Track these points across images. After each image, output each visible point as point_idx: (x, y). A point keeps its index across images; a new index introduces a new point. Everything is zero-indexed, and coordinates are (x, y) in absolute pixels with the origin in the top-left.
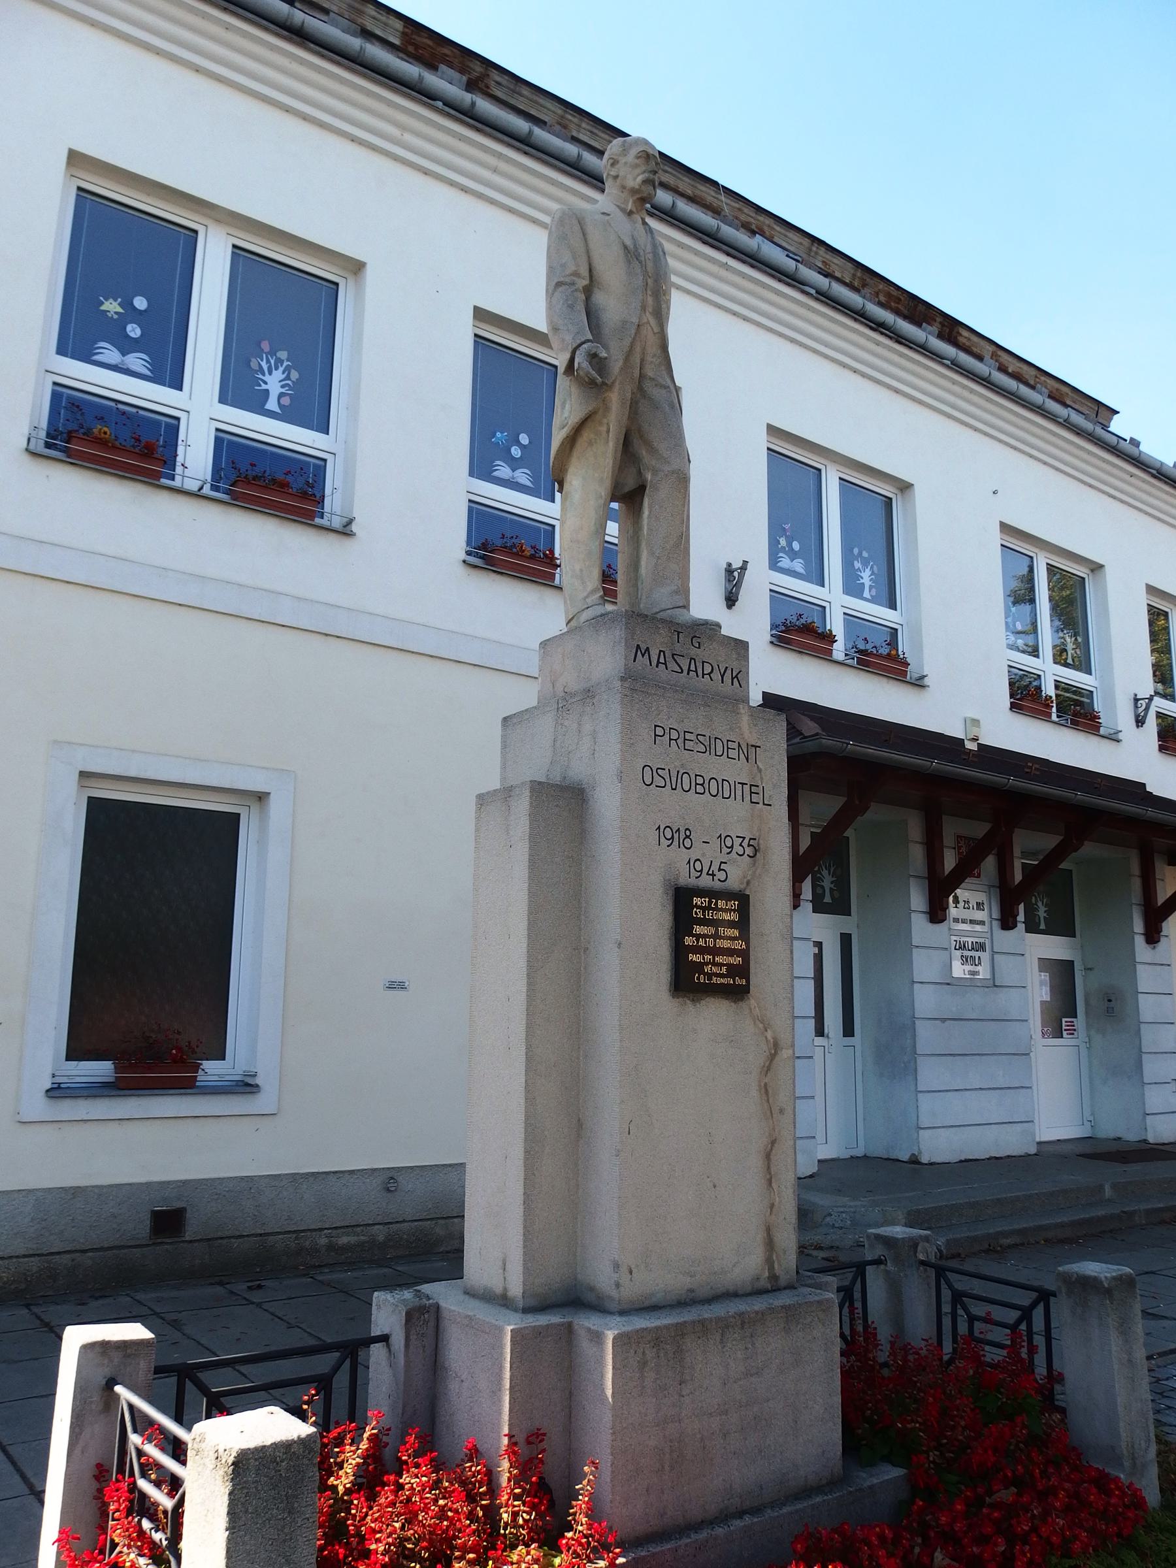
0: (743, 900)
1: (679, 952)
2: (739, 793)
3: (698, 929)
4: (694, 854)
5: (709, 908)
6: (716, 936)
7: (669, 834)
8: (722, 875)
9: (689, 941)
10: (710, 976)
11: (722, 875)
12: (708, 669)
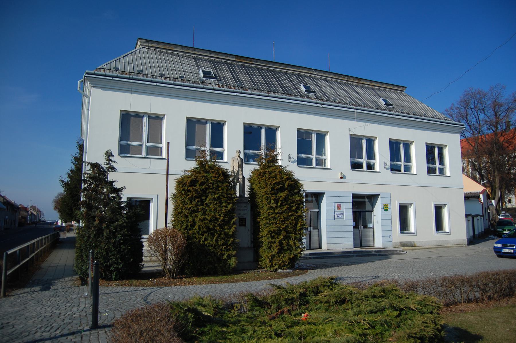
0: (245, 219)
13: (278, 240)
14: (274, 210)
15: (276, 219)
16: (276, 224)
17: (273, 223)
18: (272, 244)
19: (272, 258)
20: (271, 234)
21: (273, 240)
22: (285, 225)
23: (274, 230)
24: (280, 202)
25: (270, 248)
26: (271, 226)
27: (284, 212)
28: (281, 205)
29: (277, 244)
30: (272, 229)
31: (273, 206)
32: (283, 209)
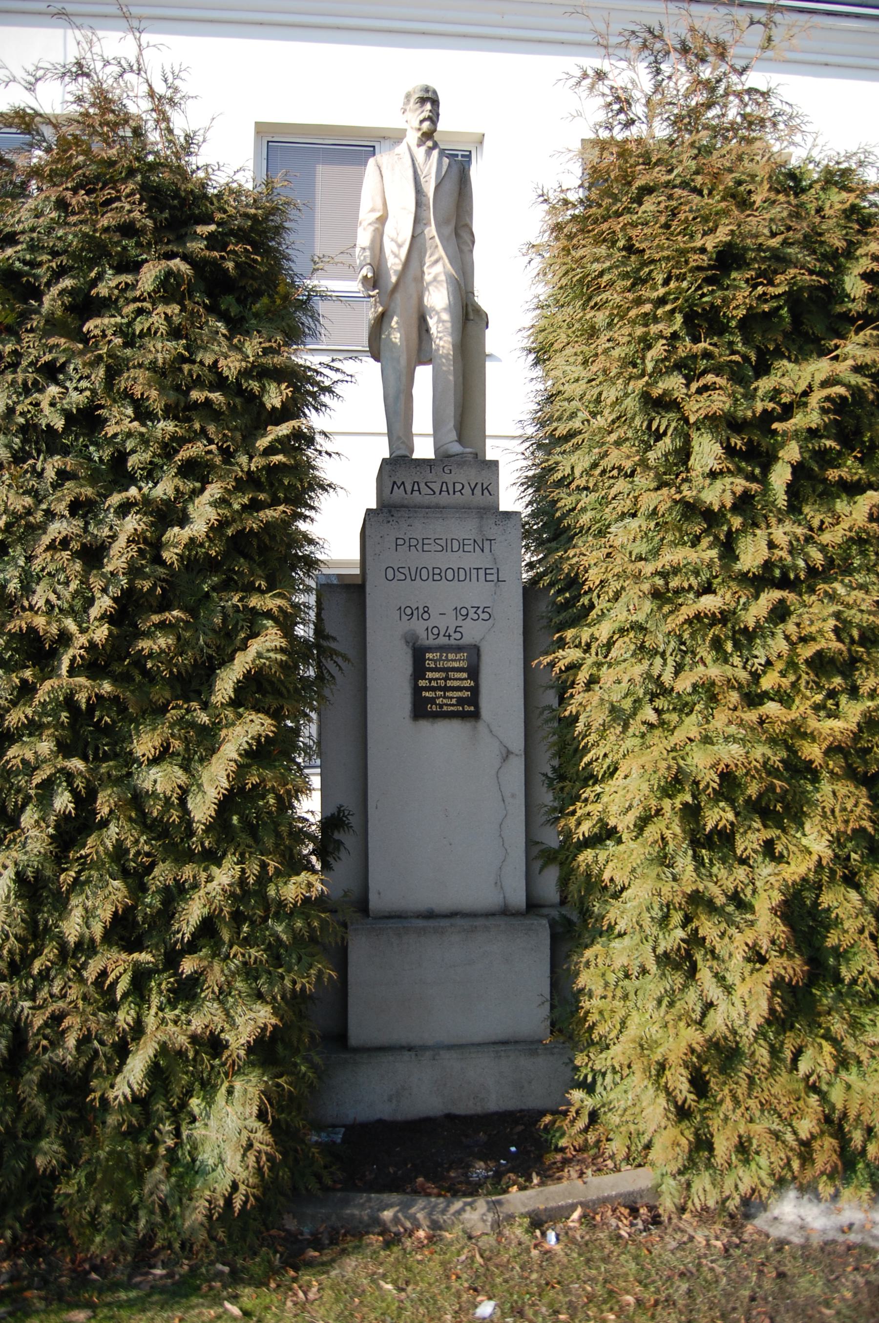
0: (475, 651)
1: (417, 691)
2: (474, 576)
3: (429, 675)
4: (430, 624)
5: (440, 659)
6: (447, 679)
7: (409, 611)
8: (458, 636)
9: (422, 683)
10: (441, 706)
11: (458, 636)
12: (458, 487)
13: (768, 886)
14: (728, 549)
15: (746, 638)
16: (753, 699)
17: (710, 693)
18: (708, 928)
19: (699, 1084)
20: (691, 813)
21: (726, 878)
22: (853, 713)
23: (727, 778)
24: (792, 452)
25: (683, 962)
26: (691, 726)
27: (836, 566)
28: (807, 484)
29: (766, 925)
30: (701, 763)
31: (716, 495)
32: (832, 537)
